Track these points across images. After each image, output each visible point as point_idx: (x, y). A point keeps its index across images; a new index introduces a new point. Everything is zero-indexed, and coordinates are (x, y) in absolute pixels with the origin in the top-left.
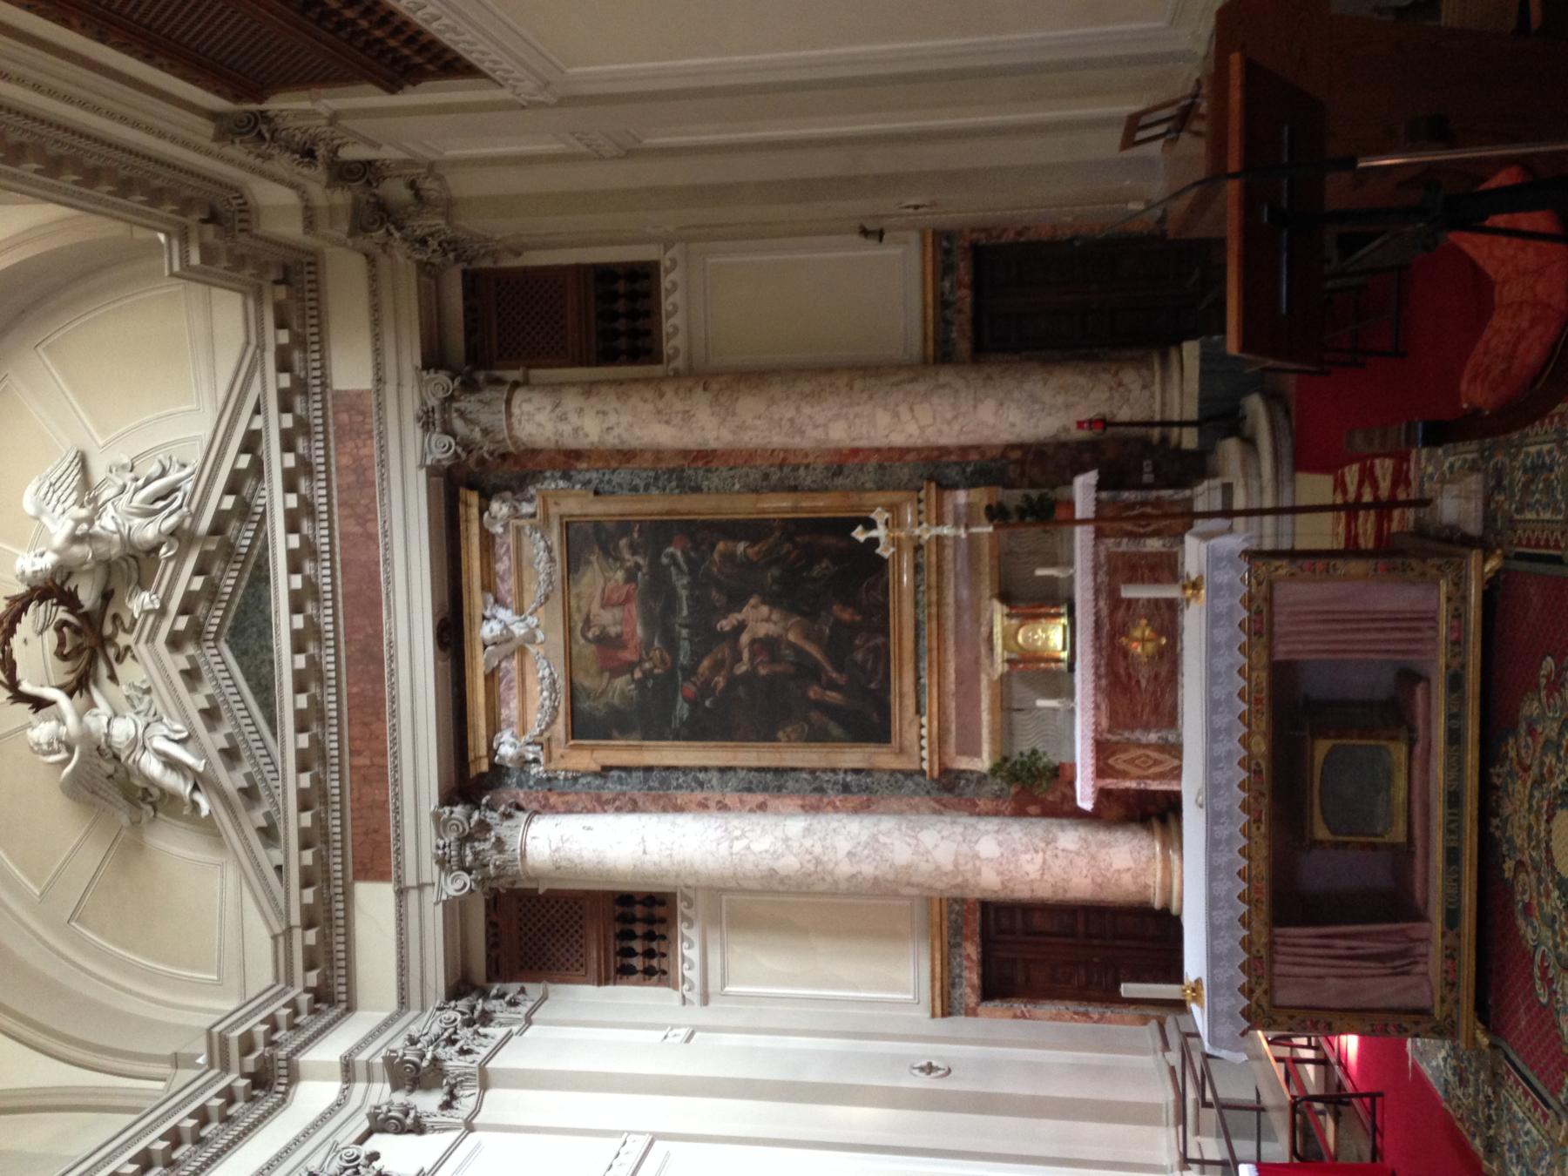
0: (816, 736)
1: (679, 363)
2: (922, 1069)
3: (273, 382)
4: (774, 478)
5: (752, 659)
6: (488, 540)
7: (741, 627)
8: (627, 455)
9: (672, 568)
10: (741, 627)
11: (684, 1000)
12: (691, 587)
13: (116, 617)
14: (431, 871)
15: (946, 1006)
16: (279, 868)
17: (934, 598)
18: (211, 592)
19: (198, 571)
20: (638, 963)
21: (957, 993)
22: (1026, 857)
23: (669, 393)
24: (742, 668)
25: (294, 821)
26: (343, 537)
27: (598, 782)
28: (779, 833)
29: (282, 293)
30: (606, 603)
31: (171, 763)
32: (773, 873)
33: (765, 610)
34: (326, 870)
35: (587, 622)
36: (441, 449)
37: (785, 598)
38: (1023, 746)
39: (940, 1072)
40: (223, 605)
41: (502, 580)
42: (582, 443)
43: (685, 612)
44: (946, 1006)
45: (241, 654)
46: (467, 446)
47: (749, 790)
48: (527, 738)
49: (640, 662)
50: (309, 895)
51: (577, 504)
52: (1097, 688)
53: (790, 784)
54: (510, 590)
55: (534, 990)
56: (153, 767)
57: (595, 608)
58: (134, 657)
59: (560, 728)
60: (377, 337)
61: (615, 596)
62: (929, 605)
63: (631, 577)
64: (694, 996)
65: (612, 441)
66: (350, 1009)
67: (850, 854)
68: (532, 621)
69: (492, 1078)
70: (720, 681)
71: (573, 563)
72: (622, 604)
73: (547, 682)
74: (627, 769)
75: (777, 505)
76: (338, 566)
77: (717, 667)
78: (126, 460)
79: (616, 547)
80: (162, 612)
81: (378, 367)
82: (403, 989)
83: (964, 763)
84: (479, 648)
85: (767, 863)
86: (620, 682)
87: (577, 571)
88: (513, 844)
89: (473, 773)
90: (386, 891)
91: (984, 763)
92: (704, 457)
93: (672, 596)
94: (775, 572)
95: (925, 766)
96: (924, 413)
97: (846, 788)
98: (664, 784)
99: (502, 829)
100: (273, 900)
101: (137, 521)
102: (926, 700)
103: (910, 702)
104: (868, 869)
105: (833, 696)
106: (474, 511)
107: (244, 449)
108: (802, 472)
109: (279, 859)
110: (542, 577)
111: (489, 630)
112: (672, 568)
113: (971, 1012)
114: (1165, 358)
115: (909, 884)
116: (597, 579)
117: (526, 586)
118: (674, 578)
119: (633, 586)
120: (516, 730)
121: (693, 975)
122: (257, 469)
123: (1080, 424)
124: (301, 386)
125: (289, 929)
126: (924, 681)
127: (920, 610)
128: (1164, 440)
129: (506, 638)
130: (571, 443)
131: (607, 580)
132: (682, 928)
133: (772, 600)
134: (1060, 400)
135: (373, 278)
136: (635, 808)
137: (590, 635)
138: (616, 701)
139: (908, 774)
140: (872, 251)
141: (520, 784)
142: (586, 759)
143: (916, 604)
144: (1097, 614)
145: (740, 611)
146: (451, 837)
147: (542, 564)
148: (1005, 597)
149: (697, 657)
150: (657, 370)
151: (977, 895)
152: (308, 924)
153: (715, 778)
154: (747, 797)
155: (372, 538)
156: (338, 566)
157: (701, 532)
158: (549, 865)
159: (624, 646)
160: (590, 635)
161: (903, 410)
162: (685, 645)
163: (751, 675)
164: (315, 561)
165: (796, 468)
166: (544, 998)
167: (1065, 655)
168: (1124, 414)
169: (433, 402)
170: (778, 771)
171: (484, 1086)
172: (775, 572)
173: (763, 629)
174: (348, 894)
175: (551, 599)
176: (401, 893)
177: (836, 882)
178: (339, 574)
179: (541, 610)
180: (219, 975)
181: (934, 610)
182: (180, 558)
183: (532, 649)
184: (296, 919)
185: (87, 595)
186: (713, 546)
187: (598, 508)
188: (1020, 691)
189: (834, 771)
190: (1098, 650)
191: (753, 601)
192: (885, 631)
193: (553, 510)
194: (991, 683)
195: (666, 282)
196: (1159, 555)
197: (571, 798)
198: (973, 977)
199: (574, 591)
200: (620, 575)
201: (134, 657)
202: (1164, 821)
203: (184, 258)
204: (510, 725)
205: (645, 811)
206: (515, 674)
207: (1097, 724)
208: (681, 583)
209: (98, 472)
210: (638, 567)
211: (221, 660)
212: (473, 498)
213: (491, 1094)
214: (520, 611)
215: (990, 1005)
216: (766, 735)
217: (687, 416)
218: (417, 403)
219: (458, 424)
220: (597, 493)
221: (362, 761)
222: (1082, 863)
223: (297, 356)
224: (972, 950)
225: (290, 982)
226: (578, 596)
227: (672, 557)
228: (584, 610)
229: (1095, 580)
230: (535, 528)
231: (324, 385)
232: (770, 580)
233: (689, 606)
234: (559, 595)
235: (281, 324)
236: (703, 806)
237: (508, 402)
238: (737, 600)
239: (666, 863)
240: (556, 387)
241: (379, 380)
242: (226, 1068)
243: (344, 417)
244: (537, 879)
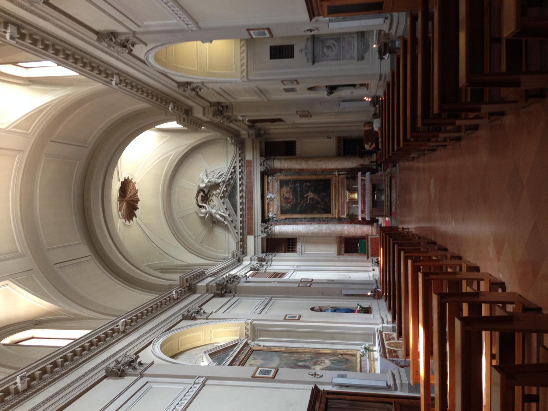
0: (320, 213)
1: (299, 156)
2: (312, 375)
3: (238, 159)
4: (313, 173)
5: (309, 201)
6: (268, 183)
7: (308, 196)
8: (290, 170)
10: (308, 196)
11: (298, 255)
12: (300, 190)
13: (210, 195)
14: (260, 233)
15: (339, 254)
16: (237, 233)
18: (227, 190)
19: (225, 187)
20: (291, 249)
21: (341, 252)
22: (351, 229)
23: (298, 161)
24: (308, 202)
25: (239, 225)
26: (247, 182)
27: (285, 221)
28: (314, 226)
29: (240, 145)
30: (287, 192)
31: (221, 216)
32: (313, 232)
33: (312, 193)
34: (243, 233)
35: (283, 196)
36: (263, 169)
37: (315, 191)
38: (351, 212)
39: (319, 376)
42: (284, 168)
43: (299, 193)
44: (339, 254)
45: (230, 200)
46: (266, 168)
47: (309, 221)
48: (274, 214)
49: (292, 201)
50: (241, 237)
51: (282, 177)
52: (362, 203)
53: (315, 220)
55: (275, 253)
56: (218, 217)
57: (285, 193)
58: (213, 201)
59: (279, 212)
60: (253, 152)
63: (290, 188)
64: (300, 254)
65: (289, 167)
66: (246, 255)
67: (325, 229)
68: (275, 195)
69: (273, 260)
70: (305, 204)
71: (282, 186)
72: (290, 192)
73: (277, 205)
74: (290, 218)
75: (314, 177)
77: (304, 203)
78: (213, 170)
79: (288, 184)
80: (220, 193)
81: (253, 156)
82: (255, 252)
83: (342, 216)
84: (267, 199)
85: (312, 231)
86: (289, 205)
88: (273, 229)
89: (265, 219)
90: (252, 237)
91: (345, 216)
92: (303, 170)
93: (297, 192)
94: (313, 188)
95: (336, 217)
96: (336, 163)
97: (324, 221)
98: (295, 221)
99: (271, 227)
100: (236, 238)
101: (216, 179)
102: (336, 207)
103: (334, 207)
104: (328, 231)
105: (322, 207)
106: (266, 178)
107: (233, 168)
108: (317, 173)
109: (237, 231)
110: (277, 188)
111: (268, 197)
113: (343, 255)
114: (371, 156)
115: (334, 233)
116: (285, 189)
120: (272, 212)
121: (300, 250)
122: (235, 172)
123: (359, 165)
124: (242, 159)
125: (238, 242)
126: (336, 204)
128: (371, 167)
129: (271, 198)
130: (282, 167)
132: (298, 243)
133: (313, 192)
134: (356, 162)
135: (253, 143)
136: (291, 224)
137: (284, 197)
138: (288, 208)
139: (334, 218)
140: (329, 140)
141: (272, 221)
142: (283, 217)
143: (335, 192)
144: (362, 192)
145: (308, 193)
146: (263, 228)
148: (348, 190)
149: (301, 201)
150: (295, 157)
151: (344, 237)
152: (241, 241)
153: (303, 220)
154: (308, 222)
155: (252, 182)
157: (302, 182)
158: (278, 232)
159: (289, 199)
160: (284, 197)
161: (333, 163)
162: (299, 199)
163: (309, 204)
165: (317, 172)
166: (276, 255)
167: (357, 198)
168: (365, 164)
169: (262, 161)
170: (314, 218)
171: (272, 261)
172: (313, 188)
173: (311, 196)
174: (246, 237)
176: (255, 237)
177: (323, 234)
180: (225, 250)
182: (223, 185)
183: (275, 200)
184: (239, 240)
185: (206, 192)
186: (303, 184)
187: (285, 178)
188: (350, 205)
189: (322, 218)
190: (362, 197)
191: (310, 192)
192: (330, 197)
193: (278, 178)
194: (346, 203)
195: (297, 144)
197: (280, 223)
198: (343, 249)
199: (281, 191)
200: (289, 188)
201: (213, 201)
202: (372, 224)
203: (232, 141)
204: (271, 212)
205: (292, 224)
206: (272, 204)
207: (362, 208)
208: (299, 189)
209: (208, 173)
210: (292, 187)
211: (227, 201)
212: (266, 176)
213: (272, 262)
214: (273, 194)
215: (346, 254)
216: (312, 213)
217: (301, 164)
218: (259, 162)
219: (265, 165)
220: (285, 175)
221: (249, 217)
222: (360, 229)
223: (241, 155)
224: (343, 245)
225: (238, 250)
227: (297, 186)
230: (275, 181)
231: (245, 159)
235: (239, 150)
236: (302, 224)
237: (273, 161)
238: (307, 192)
239: (297, 231)
240: (280, 159)
241: (253, 158)
242: (234, 258)
243: (247, 164)
244: (275, 235)
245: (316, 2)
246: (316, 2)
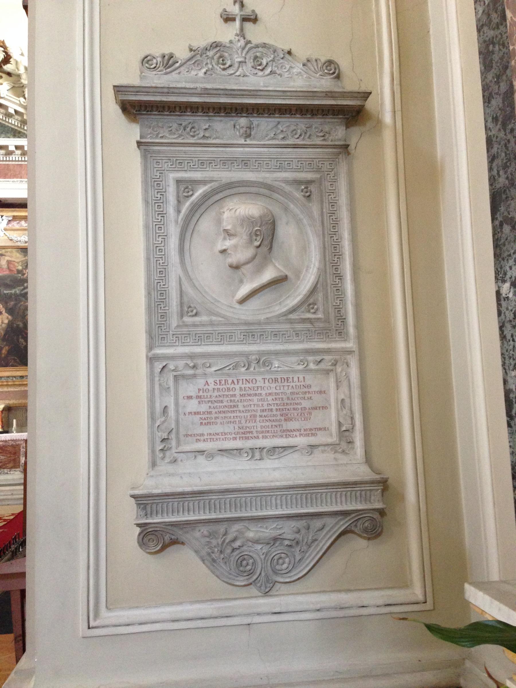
9: (23, 287)
12: (15, 294)
17: (9, 383)
19: (16, 111)
30: (9, 262)
33: (6, 321)
40: (4, 119)
41: (18, 223)
43: (5, 292)
54: (13, 225)
57: (7, 258)
61: (12, 266)
62: (7, 382)
72: (9, 268)
76: (20, 163)
87: (21, 251)
110: (19, 239)
112: (23, 287)
117: (16, 232)
118: (19, 288)
119: (16, 272)
127: (6, 378)
131: (18, 263)
143: (8, 377)
145: (6, 312)
147: (24, 239)
156: (20, 163)
164: (21, 155)
175: (11, 242)
178: (17, 163)
179: (6, 238)
181: (5, 383)
182: (21, 105)
185: (8, 67)
191: (10, 317)
196: (19, 462)
199: (14, 250)
226: (11, 252)
228: (6, 254)
229: (9, 440)
232: (19, 323)
233: (8, 293)
234: (13, 244)
245: (1, 495)
246: (1, 495)
